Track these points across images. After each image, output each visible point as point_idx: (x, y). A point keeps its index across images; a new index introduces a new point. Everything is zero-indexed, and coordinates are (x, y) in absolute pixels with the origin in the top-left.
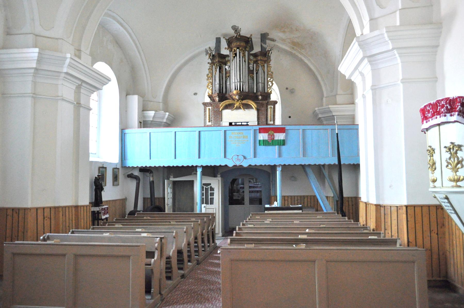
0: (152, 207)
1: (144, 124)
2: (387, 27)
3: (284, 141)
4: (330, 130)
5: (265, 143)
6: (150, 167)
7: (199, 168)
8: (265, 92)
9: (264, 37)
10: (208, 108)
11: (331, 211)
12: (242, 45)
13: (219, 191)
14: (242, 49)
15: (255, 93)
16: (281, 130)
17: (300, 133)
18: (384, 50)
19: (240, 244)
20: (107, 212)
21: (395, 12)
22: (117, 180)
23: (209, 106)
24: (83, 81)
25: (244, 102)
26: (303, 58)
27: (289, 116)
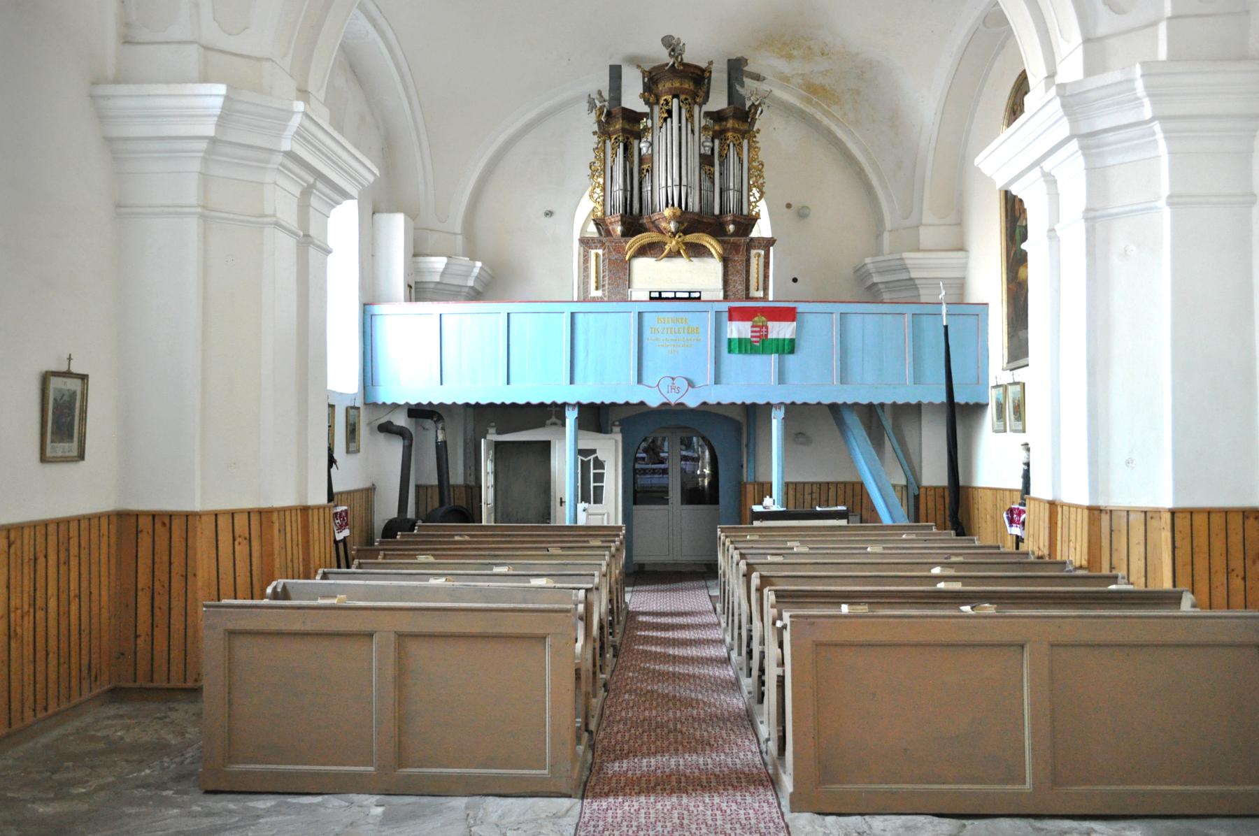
0: (444, 508)
1: (418, 291)
2: (1144, 64)
3: (792, 341)
4: (911, 316)
5: (743, 346)
6: (441, 405)
7: (571, 408)
8: (742, 214)
9: (736, 69)
10: (593, 252)
11: (906, 522)
12: (686, 89)
13: (616, 470)
14: (686, 99)
15: (717, 216)
16: (787, 314)
18: (1126, 122)
19: (925, 605)
20: (347, 524)
21: (1154, 24)
22: (354, 438)
23: (596, 248)
24: (320, 176)
25: (691, 238)
26: (834, 127)
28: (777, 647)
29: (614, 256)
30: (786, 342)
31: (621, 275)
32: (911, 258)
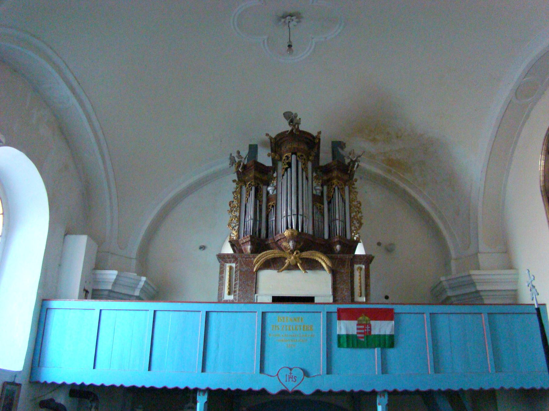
3: (391, 337)
6: (92, 385)
7: (201, 394)
10: (228, 265)
14: (302, 156)
15: (327, 240)
23: (230, 262)
25: (305, 254)
26: (408, 189)
27: (384, 296)
28: (229, 205)
29: (245, 268)
30: (387, 337)
32: (477, 275)
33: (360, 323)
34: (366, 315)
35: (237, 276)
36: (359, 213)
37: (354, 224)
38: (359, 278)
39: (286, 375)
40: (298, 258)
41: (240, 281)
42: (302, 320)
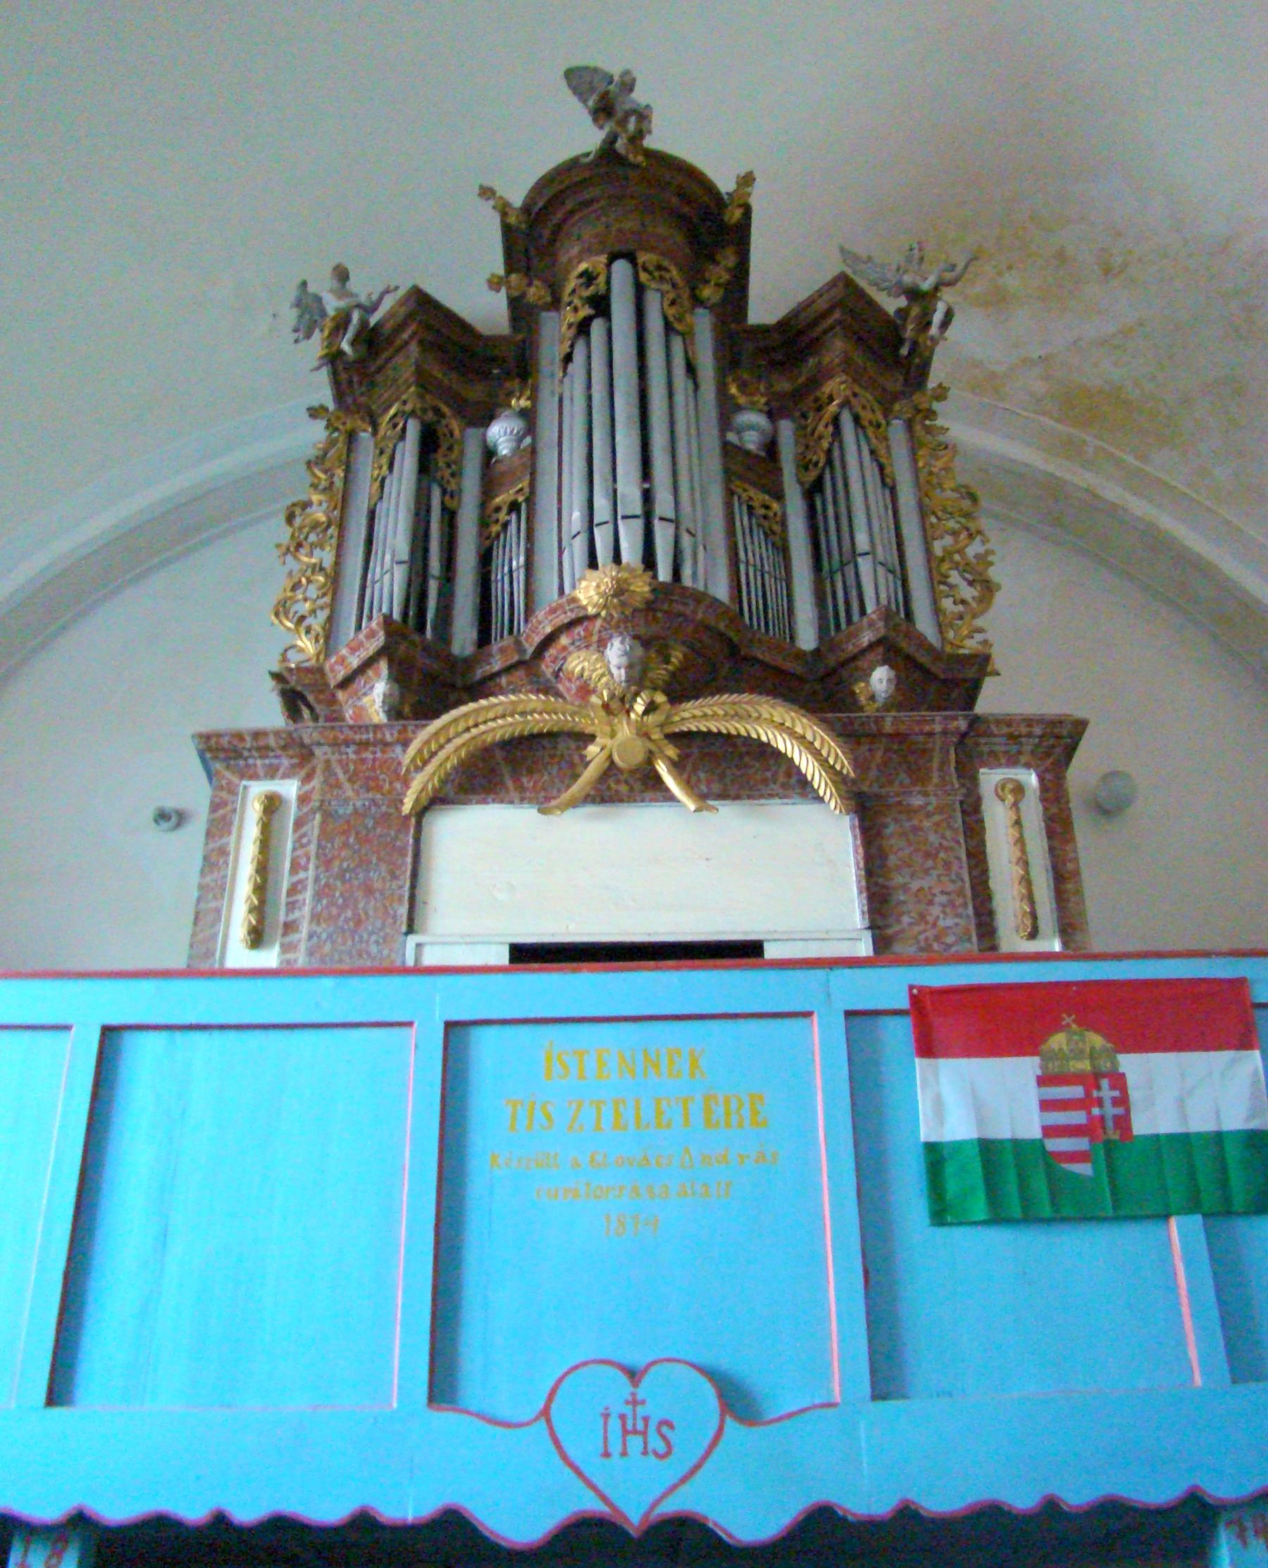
10: (257, 790)
17: (1173, 1287)
23: (272, 773)
26: (1167, 522)
30: (1233, 1153)
31: (377, 876)
33: (1054, 1067)
34: (1087, 1023)
35: (309, 842)
36: (971, 536)
37: (951, 586)
38: (1010, 823)
39: (606, 1416)
40: (656, 736)
41: (322, 869)
42: (694, 1064)
